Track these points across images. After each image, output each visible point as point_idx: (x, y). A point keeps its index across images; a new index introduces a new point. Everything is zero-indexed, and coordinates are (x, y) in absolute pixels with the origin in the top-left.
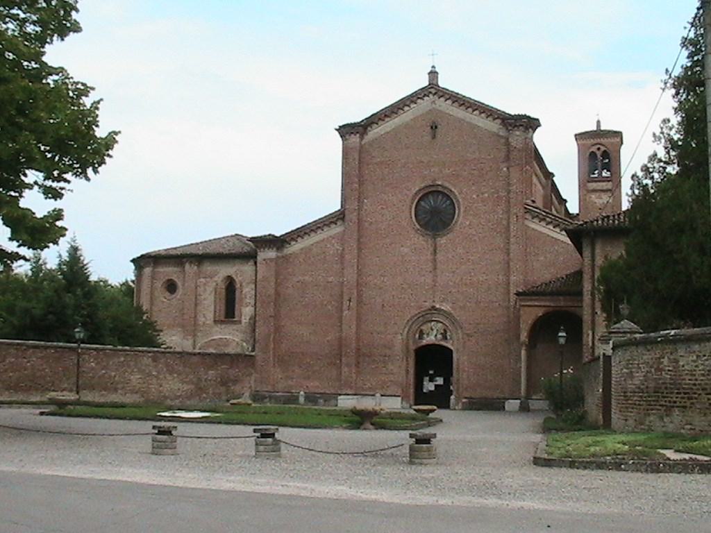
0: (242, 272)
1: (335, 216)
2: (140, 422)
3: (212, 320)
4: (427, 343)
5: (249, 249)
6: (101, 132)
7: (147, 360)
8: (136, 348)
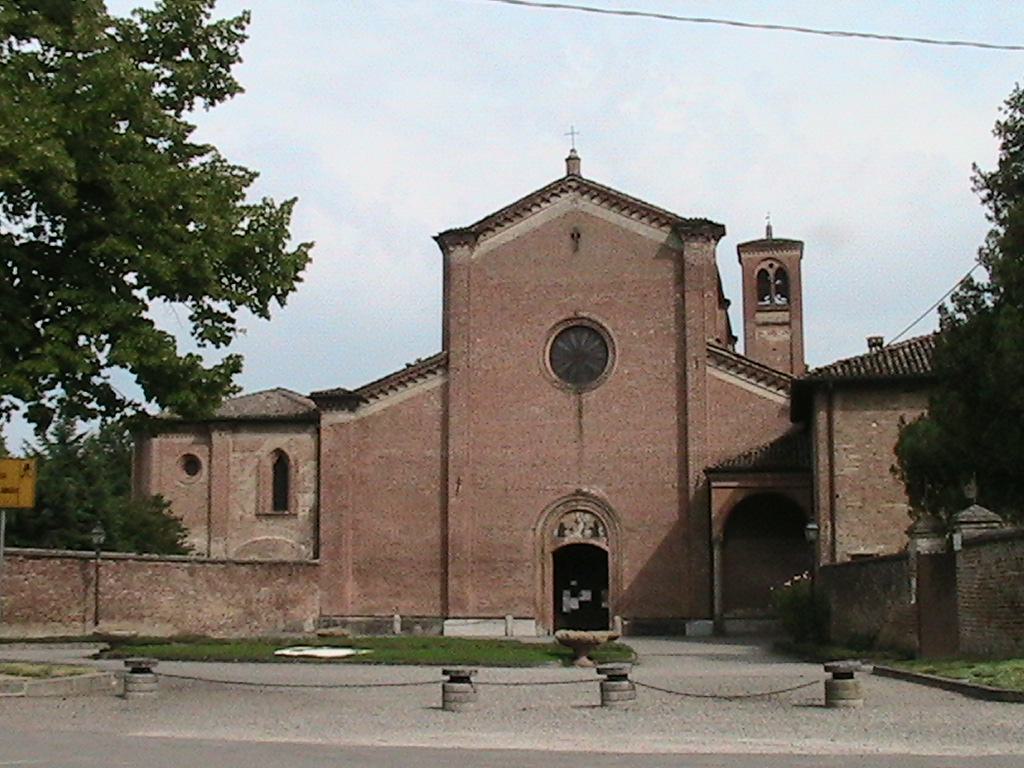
0: (297, 444)
1: (435, 363)
2: (894, 682)
3: (253, 513)
4: (572, 541)
5: (306, 409)
6: (290, 247)
7: (182, 574)
8: (168, 557)
